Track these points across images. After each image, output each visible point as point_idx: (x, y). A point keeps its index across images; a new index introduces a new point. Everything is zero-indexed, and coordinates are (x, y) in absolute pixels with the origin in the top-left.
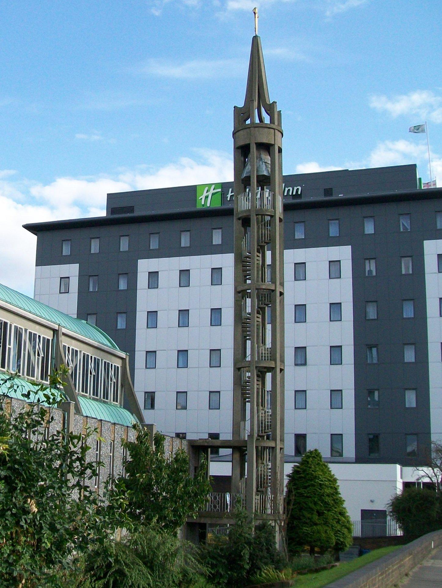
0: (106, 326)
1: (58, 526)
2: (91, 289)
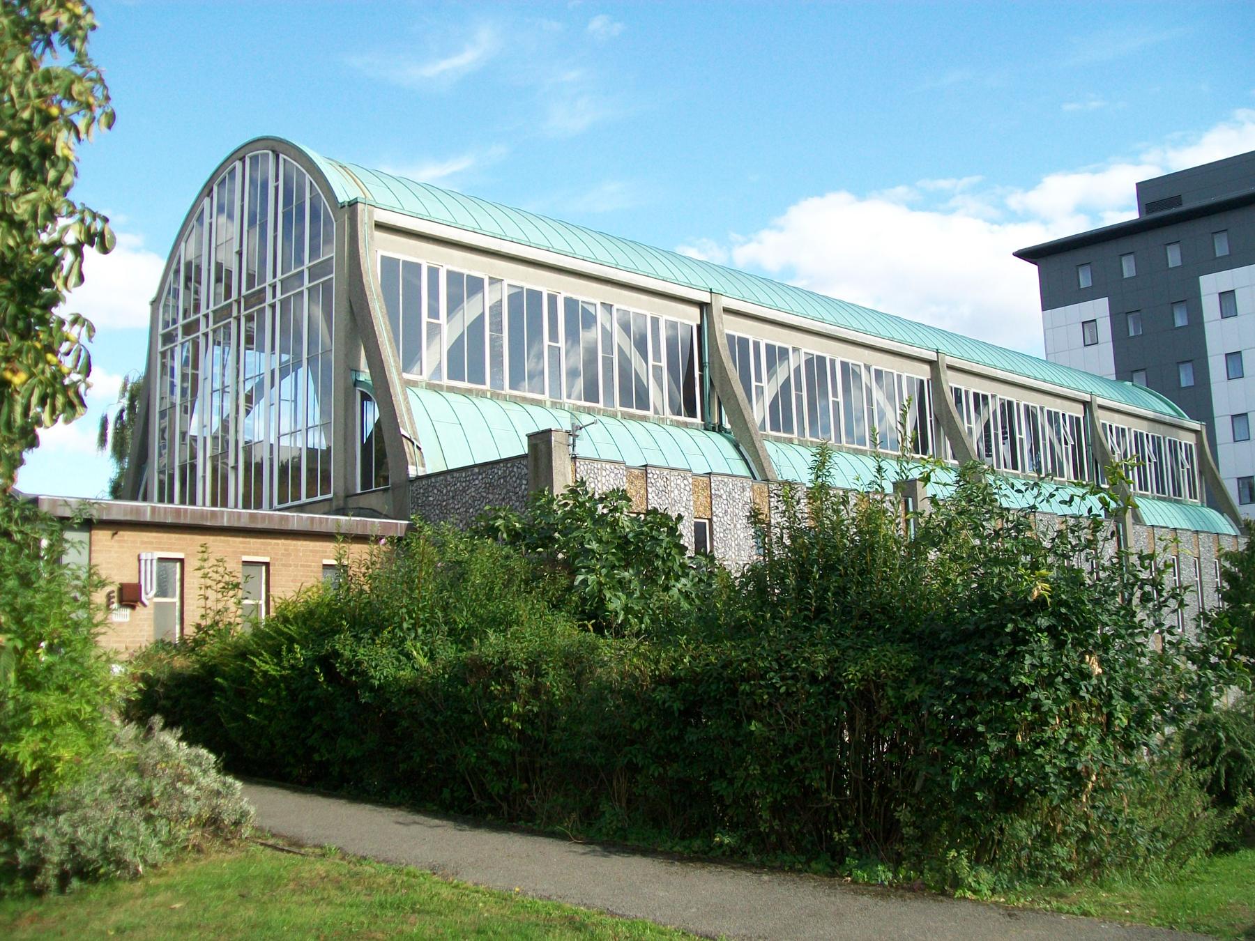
0: (1162, 385)
1: (1136, 692)
2: (1132, 334)
